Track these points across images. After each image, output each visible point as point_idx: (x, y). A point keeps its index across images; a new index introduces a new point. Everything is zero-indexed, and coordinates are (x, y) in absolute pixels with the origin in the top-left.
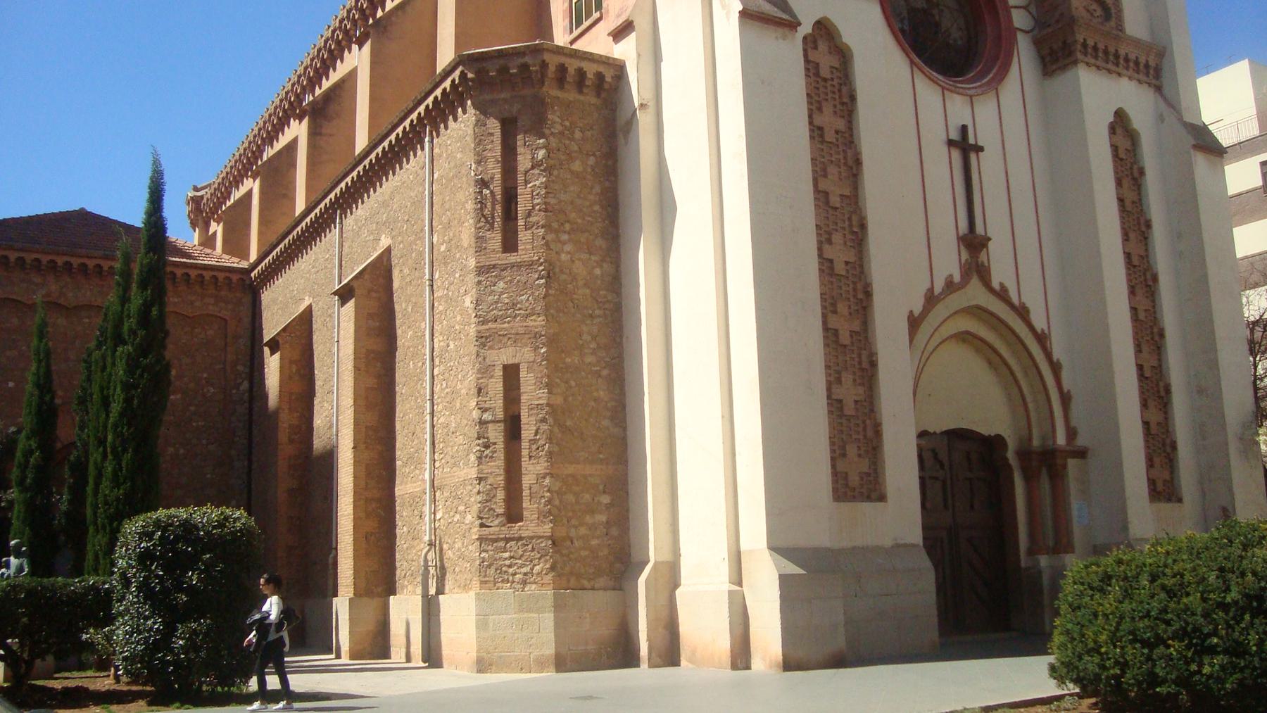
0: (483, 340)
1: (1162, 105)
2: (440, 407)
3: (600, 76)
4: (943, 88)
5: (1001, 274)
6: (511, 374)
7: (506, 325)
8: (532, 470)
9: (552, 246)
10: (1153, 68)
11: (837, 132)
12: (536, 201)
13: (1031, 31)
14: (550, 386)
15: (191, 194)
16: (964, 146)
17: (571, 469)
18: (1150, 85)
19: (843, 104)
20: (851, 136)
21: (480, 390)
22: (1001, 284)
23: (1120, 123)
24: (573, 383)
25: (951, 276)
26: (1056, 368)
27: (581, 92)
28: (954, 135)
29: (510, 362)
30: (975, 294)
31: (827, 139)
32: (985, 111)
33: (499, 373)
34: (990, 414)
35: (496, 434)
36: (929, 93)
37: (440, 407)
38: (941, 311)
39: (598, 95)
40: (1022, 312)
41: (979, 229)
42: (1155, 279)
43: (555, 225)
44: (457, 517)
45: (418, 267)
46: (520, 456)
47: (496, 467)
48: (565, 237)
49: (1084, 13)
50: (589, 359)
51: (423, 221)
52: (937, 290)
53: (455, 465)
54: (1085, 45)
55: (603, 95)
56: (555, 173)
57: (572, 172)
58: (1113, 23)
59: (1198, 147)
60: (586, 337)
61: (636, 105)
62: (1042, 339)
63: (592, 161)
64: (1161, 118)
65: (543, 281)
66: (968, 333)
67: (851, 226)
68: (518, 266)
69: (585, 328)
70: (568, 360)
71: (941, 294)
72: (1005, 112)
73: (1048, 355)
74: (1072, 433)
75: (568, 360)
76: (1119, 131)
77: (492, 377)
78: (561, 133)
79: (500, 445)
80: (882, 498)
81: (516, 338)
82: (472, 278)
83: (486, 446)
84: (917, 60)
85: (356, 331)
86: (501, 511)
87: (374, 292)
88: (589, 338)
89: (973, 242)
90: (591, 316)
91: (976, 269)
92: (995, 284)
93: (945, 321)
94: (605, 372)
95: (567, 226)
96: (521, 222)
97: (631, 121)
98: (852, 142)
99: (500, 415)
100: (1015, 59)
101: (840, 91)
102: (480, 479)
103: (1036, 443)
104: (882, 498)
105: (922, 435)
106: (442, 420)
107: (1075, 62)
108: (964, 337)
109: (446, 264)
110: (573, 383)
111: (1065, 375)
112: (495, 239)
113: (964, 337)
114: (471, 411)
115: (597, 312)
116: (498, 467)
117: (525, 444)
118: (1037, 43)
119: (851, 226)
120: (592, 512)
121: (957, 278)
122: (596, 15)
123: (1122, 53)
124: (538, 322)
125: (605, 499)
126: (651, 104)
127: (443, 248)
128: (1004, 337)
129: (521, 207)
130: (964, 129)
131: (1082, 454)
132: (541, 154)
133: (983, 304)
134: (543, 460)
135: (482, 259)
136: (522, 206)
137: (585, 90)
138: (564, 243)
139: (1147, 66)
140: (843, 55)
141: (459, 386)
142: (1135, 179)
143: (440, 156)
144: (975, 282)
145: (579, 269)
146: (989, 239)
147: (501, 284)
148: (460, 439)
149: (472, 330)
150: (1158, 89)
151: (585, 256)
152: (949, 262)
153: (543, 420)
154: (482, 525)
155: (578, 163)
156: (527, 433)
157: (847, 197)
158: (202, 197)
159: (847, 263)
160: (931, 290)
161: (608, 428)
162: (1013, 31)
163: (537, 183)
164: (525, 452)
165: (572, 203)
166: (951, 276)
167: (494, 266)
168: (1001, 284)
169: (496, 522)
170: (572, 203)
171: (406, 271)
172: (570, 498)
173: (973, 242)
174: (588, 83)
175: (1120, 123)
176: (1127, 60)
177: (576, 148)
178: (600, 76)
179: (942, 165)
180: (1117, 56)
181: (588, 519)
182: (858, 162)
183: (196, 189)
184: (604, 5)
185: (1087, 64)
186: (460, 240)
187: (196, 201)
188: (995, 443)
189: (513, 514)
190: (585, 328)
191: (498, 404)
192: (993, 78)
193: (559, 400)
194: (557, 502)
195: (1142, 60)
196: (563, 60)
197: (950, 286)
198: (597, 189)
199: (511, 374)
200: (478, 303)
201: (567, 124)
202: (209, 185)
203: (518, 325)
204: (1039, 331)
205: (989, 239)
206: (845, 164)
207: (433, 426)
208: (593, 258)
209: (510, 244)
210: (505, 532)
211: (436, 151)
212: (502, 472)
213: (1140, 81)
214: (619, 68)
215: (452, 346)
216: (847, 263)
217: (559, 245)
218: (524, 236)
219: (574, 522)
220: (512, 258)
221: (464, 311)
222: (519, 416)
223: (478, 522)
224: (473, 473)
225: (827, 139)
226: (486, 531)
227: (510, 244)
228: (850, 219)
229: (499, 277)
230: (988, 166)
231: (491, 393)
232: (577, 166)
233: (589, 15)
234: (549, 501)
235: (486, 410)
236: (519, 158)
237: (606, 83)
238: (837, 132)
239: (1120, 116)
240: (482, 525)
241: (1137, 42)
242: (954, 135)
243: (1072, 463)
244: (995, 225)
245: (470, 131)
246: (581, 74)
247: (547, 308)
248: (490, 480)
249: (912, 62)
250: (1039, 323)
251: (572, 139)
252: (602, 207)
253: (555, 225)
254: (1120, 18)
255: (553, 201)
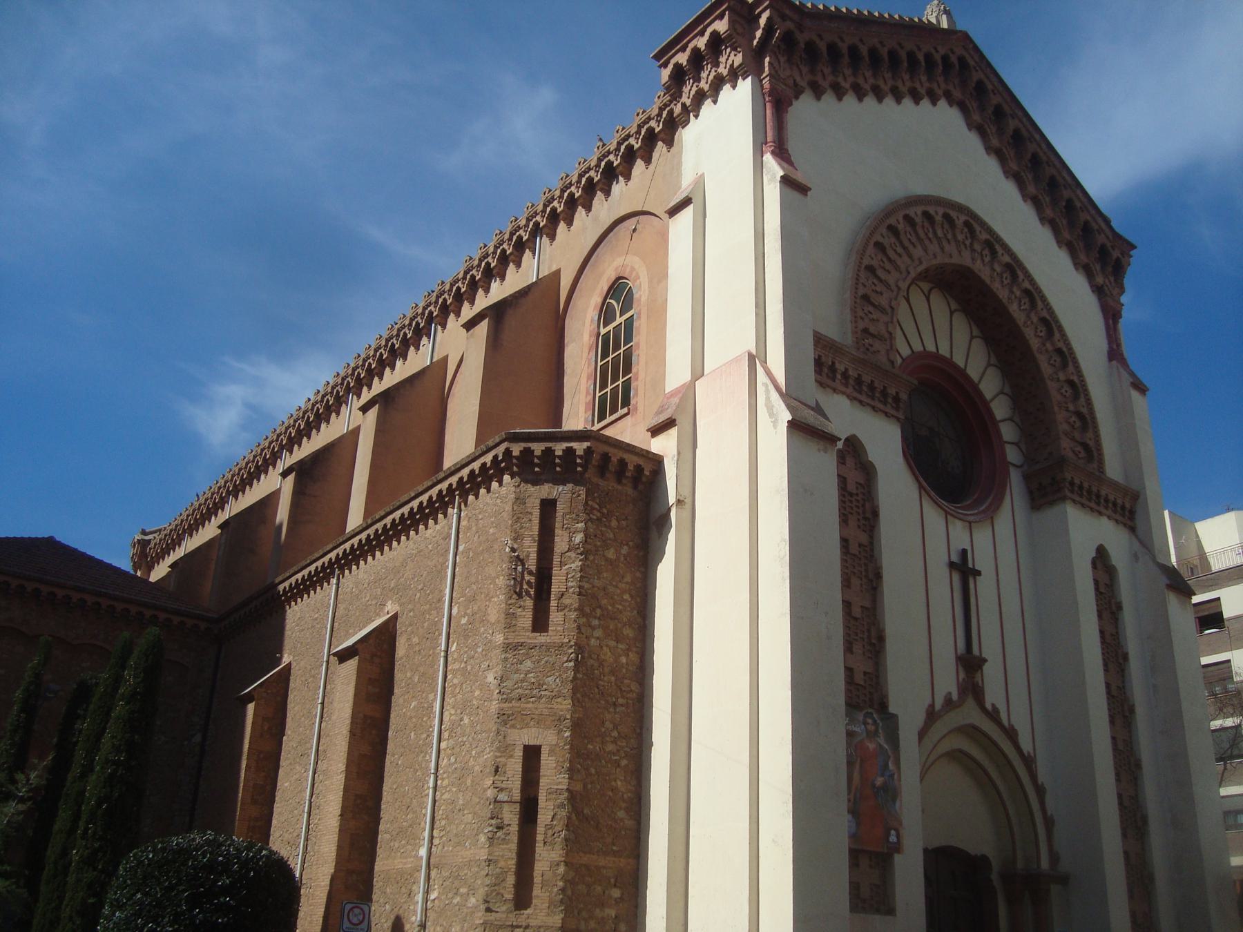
0: (504, 718)
1: (1137, 545)
2: (446, 782)
3: (639, 469)
4: (946, 513)
5: (993, 695)
6: (532, 754)
7: (530, 705)
8: (548, 857)
9: (583, 630)
10: (1127, 508)
11: (860, 545)
12: (570, 584)
13: (1021, 466)
14: (572, 771)
15: (138, 537)
16: (963, 569)
17: (586, 859)
18: (1125, 525)
19: (866, 519)
20: (872, 550)
21: (497, 771)
22: (993, 705)
23: (1101, 558)
24: (593, 771)
25: (950, 693)
26: (1040, 791)
27: (619, 482)
28: (955, 558)
29: (531, 743)
30: (970, 714)
31: (852, 551)
32: (982, 537)
33: (519, 753)
34: (976, 834)
35: (511, 816)
36: (934, 517)
37: (446, 782)
38: (940, 728)
39: (635, 487)
40: (1011, 734)
41: (976, 651)
42: (1132, 710)
43: (587, 609)
44: (457, 900)
45: (432, 635)
46: (534, 841)
47: (508, 852)
48: (595, 622)
49: (1071, 454)
50: (611, 747)
51: (442, 591)
52: (938, 706)
53: (459, 844)
54: (1072, 484)
55: (641, 487)
56: (591, 558)
57: (607, 560)
58: (1095, 465)
59: (1170, 587)
60: (609, 725)
61: (672, 499)
62: (1029, 762)
63: (625, 550)
64: (1135, 557)
65: (572, 664)
66: (961, 751)
67: (869, 637)
68: (547, 647)
69: (608, 716)
70: (590, 746)
71: (940, 711)
72: (999, 541)
73: (1033, 777)
74: (1054, 858)
75: (590, 746)
76: (1099, 565)
77: (511, 756)
78: (599, 519)
79: (515, 828)
80: (891, 911)
81: (540, 721)
82: (497, 655)
83: (499, 828)
84: (924, 484)
85: (355, 695)
86: (510, 896)
87: (377, 658)
88: (611, 726)
89: (970, 663)
90: (614, 704)
91: (972, 688)
92: (988, 706)
93: (944, 736)
94: (624, 762)
95: (599, 612)
96: (553, 603)
97: (666, 517)
98: (872, 556)
99: (517, 795)
100: (1008, 491)
101: (863, 506)
102: (489, 862)
103: (1020, 865)
104: (891, 911)
105: (926, 851)
106: (446, 796)
107: (1064, 499)
108: (956, 756)
109: (466, 637)
110: (593, 771)
111: (1049, 799)
112: (526, 618)
113: (956, 756)
114: (485, 790)
115: (621, 701)
116: (510, 850)
117: (540, 829)
118: (1027, 478)
119: (869, 637)
120: (602, 905)
121: (955, 696)
122: (622, 412)
123: (1103, 493)
124: (564, 706)
125: (616, 893)
126: (688, 501)
127: (464, 621)
128: (988, 755)
129: (554, 589)
130: (964, 552)
131: (1064, 880)
132: (579, 538)
133: (977, 723)
134: (558, 847)
135: (511, 636)
136: (557, 585)
137: (624, 481)
138: (593, 628)
139: (1123, 508)
140: (868, 470)
141: (471, 763)
142: (1113, 613)
143: (469, 528)
144: (971, 702)
145: (607, 655)
146: (985, 661)
147: (528, 664)
148: (469, 818)
149: (494, 706)
150: (1133, 529)
151: (612, 643)
152: (948, 681)
153: (562, 806)
154: (488, 910)
155: (612, 550)
156: (545, 814)
157: (867, 608)
158: (149, 541)
159: (865, 673)
160: (932, 706)
161: (622, 820)
162: (1006, 464)
163: (573, 566)
164: (540, 838)
165: (604, 589)
166: (950, 693)
167: (522, 644)
168: (993, 705)
169: (504, 908)
170: (604, 589)
171: (415, 640)
172: (582, 888)
173: (970, 663)
174: (629, 474)
175: (1101, 558)
176: (1107, 500)
177: (611, 536)
178: (639, 469)
179: (943, 585)
180: (1098, 496)
181: (598, 912)
182: (879, 576)
183: (144, 533)
184: (632, 402)
185: (1074, 501)
186: (486, 614)
187: (144, 544)
188: (979, 863)
189: (522, 899)
190: (608, 716)
191: (515, 784)
192: (990, 505)
193: (578, 787)
194: (569, 892)
195: (1119, 501)
196: (607, 449)
197: (949, 703)
198: (628, 578)
199: (532, 754)
200: (502, 679)
201: (605, 511)
202: (160, 530)
203: (542, 707)
204: (1025, 752)
205: (985, 661)
206: (866, 576)
207: (434, 801)
208: (620, 646)
209: (540, 623)
210: (512, 919)
211: (464, 523)
212: (514, 856)
213: (1117, 521)
214: (658, 461)
215: (466, 720)
216: (865, 673)
217: (589, 630)
218: (555, 617)
219: (584, 914)
220: (541, 638)
221: (484, 687)
222: (536, 800)
223: (483, 907)
224: (483, 854)
225: (852, 551)
226: (492, 917)
227: (540, 623)
228: (869, 631)
229: (528, 656)
230: (984, 588)
231: (509, 774)
232: (611, 554)
233: (614, 410)
234: (563, 890)
235: (502, 790)
236: (557, 539)
237: (644, 476)
238: (860, 545)
239: (1101, 552)
240: (488, 910)
241: (1114, 485)
242: (955, 558)
243: (1055, 889)
244: (989, 647)
245: (508, 507)
246: (623, 464)
247: (575, 690)
248: (502, 864)
249: (921, 487)
250: (1026, 746)
251: (609, 527)
252: (631, 596)
253: (587, 609)
254: (1101, 462)
255: (586, 586)
